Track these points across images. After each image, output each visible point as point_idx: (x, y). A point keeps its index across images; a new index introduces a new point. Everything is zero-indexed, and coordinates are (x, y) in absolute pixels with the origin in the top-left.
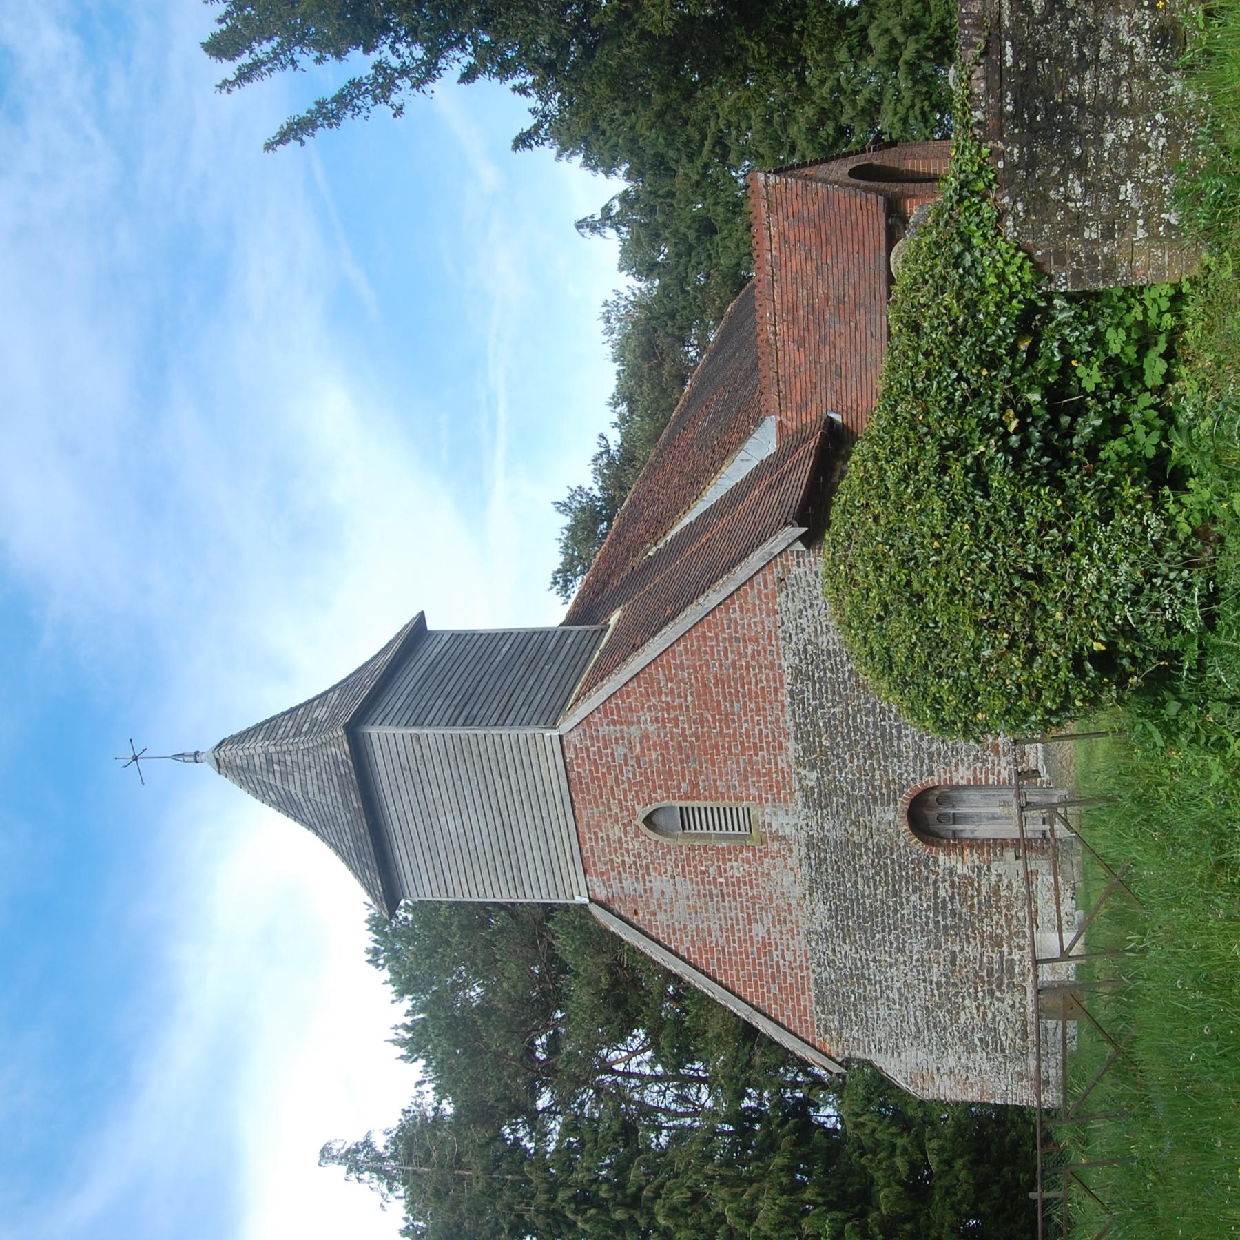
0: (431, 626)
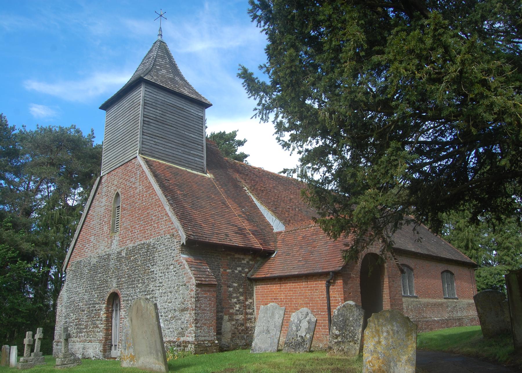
0: (207, 111)
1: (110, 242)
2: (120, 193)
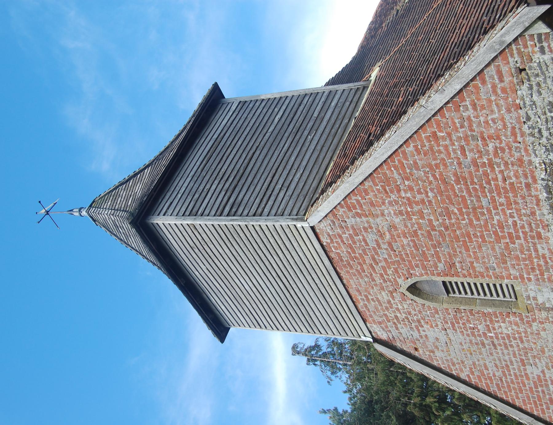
0: (228, 93)
1: (544, 314)
2: (410, 282)
